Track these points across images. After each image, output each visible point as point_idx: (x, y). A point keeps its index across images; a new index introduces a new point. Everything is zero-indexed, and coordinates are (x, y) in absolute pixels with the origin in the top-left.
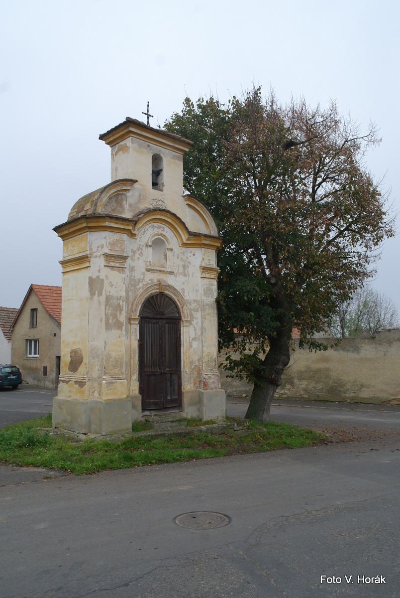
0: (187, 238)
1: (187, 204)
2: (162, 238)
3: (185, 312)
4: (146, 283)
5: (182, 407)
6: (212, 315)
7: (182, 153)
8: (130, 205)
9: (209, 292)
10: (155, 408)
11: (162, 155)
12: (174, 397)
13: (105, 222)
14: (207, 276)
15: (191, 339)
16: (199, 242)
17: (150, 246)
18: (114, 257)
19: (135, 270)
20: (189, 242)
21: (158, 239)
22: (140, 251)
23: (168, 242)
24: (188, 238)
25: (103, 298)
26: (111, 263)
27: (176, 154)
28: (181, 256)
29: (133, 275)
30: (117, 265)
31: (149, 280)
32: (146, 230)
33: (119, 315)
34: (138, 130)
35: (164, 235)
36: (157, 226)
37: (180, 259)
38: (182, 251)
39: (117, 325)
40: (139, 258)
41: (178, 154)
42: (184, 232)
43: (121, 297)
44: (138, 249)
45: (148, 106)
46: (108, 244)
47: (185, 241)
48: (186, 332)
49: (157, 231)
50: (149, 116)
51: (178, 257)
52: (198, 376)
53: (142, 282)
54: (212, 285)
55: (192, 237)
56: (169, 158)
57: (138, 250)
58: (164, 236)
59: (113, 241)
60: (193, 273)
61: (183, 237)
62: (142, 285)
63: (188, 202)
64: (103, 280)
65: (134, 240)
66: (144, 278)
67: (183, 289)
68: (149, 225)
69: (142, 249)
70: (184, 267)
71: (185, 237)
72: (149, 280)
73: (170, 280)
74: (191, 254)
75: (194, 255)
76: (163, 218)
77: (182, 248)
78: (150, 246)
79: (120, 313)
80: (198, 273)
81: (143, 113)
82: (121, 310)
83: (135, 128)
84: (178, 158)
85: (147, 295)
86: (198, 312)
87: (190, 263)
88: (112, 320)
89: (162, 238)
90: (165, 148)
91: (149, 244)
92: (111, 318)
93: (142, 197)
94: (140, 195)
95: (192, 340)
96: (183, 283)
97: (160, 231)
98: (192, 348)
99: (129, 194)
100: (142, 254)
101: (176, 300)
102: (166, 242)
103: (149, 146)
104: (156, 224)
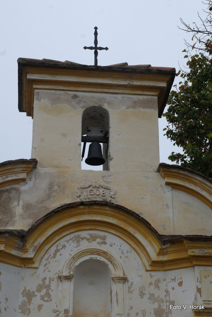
0: (158, 250)
1: (168, 184)
2: (99, 258)
7: (157, 93)
8: (27, 207)
11: (106, 106)
16: (182, 255)
17: (68, 278)
20: (165, 258)
21: (91, 260)
22: (44, 292)
23: (113, 265)
24: (161, 250)
27: (141, 97)
28: (152, 289)
32: (60, 247)
34: (44, 75)
35: (104, 253)
36: (88, 237)
37: (147, 296)
38: (153, 280)
41: (145, 97)
42: (150, 239)
44: (39, 289)
45: (96, 34)
47: (154, 257)
50: (96, 49)
51: (142, 294)
55: (168, 245)
56: (124, 107)
57: (39, 290)
58: (104, 254)
61: (150, 249)
63: (167, 180)
65: (33, 271)
68: (68, 238)
69: (48, 287)
74: (175, 284)
75: (180, 284)
76: (98, 218)
77: (153, 273)
78: (68, 278)
81: (107, 49)
83: (39, 73)
84: (145, 104)
89: (99, 258)
90: (112, 93)
91: (64, 274)
93: (55, 188)
94: (51, 186)
97: (94, 245)
99: (23, 188)
102: (110, 266)
104: (84, 234)
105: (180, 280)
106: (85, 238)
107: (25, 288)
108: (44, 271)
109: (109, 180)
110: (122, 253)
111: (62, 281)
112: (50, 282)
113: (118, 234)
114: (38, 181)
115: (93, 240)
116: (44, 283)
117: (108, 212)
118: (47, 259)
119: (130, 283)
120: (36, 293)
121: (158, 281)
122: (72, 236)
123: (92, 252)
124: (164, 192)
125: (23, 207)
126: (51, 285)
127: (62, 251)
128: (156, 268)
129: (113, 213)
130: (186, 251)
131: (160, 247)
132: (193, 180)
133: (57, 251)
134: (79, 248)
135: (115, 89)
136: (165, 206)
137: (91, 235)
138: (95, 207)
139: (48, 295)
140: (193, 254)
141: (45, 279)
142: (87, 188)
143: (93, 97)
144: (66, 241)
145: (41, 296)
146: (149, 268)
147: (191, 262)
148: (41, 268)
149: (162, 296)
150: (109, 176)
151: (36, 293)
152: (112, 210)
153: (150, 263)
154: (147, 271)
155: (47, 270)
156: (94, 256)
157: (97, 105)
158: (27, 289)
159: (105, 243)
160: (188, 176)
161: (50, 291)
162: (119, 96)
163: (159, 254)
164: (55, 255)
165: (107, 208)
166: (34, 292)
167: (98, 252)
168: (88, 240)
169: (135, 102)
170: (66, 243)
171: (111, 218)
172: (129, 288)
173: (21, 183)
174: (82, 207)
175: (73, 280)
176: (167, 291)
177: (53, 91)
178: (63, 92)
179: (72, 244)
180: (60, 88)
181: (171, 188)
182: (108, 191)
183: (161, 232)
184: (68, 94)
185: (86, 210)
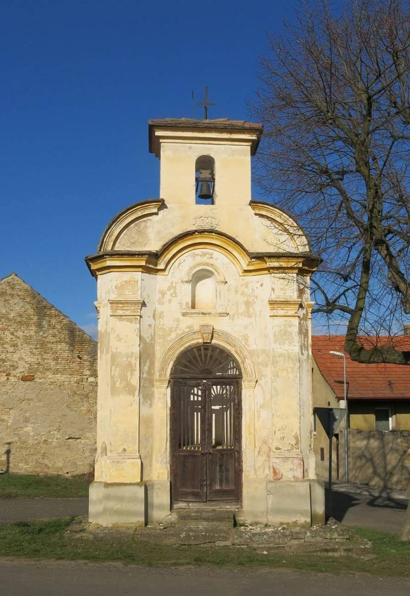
0: (248, 263)
1: (256, 214)
3: (248, 367)
4: (182, 331)
5: (241, 502)
6: (290, 370)
9: (285, 337)
10: (194, 500)
12: (225, 487)
13: (106, 261)
14: (281, 312)
15: (259, 406)
18: (122, 303)
19: (163, 316)
22: (172, 291)
23: (218, 273)
25: (109, 356)
26: (118, 311)
29: (161, 324)
30: (128, 313)
31: (186, 328)
33: (129, 377)
39: (127, 389)
40: (170, 301)
43: (132, 353)
44: (169, 289)
46: (114, 288)
48: (250, 396)
49: (199, 259)
51: (236, 292)
52: (267, 459)
53: (176, 330)
54: (290, 326)
57: (169, 289)
59: (121, 283)
60: (260, 312)
61: (242, 261)
62: (175, 335)
64: (109, 333)
66: (178, 325)
67: (246, 338)
69: (175, 288)
70: (247, 304)
71: (244, 262)
72: (186, 328)
73: (221, 325)
75: (262, 285)
79: (132, 375)
80: (267, 310)
82: (133, 370)
85: (182, 348)
86: (267, 367)
87: (256, 297)
88: (121, 383)
92: (119, 381)
95: (260, 408)
96: (246, 328)
98: (261, 418)
100: (176, 294)
101: (233, 352)
102: (216, 273)
103: (190, 148)
105: (262, 283)
118: (173, 269)
120: (167, 292)
141: (172, 282)
159: (212, 258)
164: (179, 266)
176: (253, 290)
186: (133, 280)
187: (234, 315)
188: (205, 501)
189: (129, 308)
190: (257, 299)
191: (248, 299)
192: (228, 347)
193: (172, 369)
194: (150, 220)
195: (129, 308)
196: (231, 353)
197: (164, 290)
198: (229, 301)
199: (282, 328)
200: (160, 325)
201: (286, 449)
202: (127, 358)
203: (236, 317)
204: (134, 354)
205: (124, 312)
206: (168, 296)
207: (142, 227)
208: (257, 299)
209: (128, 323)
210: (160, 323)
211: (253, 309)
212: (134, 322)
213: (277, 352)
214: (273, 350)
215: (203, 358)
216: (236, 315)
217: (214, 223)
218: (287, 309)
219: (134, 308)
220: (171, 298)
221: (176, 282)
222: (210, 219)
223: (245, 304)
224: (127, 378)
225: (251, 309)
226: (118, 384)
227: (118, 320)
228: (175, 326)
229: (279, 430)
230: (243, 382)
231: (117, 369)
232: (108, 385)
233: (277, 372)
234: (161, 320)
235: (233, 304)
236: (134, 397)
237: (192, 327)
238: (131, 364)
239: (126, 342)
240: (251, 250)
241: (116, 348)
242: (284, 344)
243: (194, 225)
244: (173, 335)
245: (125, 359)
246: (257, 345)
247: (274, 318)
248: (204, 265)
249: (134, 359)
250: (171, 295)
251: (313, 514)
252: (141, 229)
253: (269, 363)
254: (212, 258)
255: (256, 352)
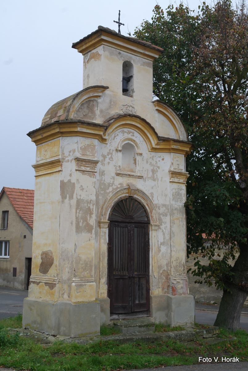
0: (156, 143)
1: (157, 110)
3: (154, 216)
5: (150, 312)
8: (101, 111)
11: (132, 62)
15: (159, 243)
16: (168, 147)
17: (120, 151)
18: (85, 162)
19: (105, 174)
20: (158, 147)
21: (128, 143)
22: (110, 156)
23: (137, 147)
24: (158, 143)
25: (74, 202)
26: (82, 167)
28: (150, 160)
29: (103, 179)
30: (88, 169)
31: (119, 184)
32: (116, 135)
33: (89, 219)
34: (109, 38)
35: (134, 141)
36: (127, 131)
37: (149, 163)
39: (87, 228)
40: (109, 163)
41: (148, 61)
47: (154, 146)
50: (120, 24)
51: (147, 162)
53: (112, 186)
55: (161, 141)
57: (108, 155)
58: (134, 141)
60: (162, 178)
63: (157, 108)
65: (105, 145)
66: (113, 182)
68: (119, 131)
69: (112, 154)
70: (153, 171)
71: (154, 142)
72: (119, 184)
73: (140, 185)
74: (160, 159)
75: (163, 159)
77: (151, 153)
78: (120, 151)
80: (167, 178)
82: (91, 214)
84: (148, 65)
86: (167, 216)
87: (159, 167)
88: (83, 223)
90: (135, 55)
93: (112, 103)
95: (161, 245)
99: (100, 100)
102: (136, 147)
104: (126, 130)
105: (163, 158)
106: (126, 132)
107: (102, 153)
108: (110, 146)
109: (134, 103)
110: (140, 142)
111: (117, 152)
112: (112, 151)
113: (139, 132)
114: (105, 98)
115: (129, 134)
116: (110, 152)
117: (138, 121)
118: (111, 140)
119: (143, 156)
120: (107, 156)
121: (153, 157)
122: (121, 130)
123: (129, 139)
124: (155, 114)
125: (100, 111)
126: (113, 153)
127: (117, 137)
128: (153, 151)
129: (140, 122)
130: (170, 145)
131: (158, 142)
132: (168, 110)
133: (115, 137)
134: (124, 136)
135: (137, 53)
136: (155, 121)
137: (128, 131)
138: (134, 118)
139: (112, 157)
140: (173, 148)
141: (110, 150)
142: (125, 106)
143: (127, 56)
144: (118, 132)
145: (109, 158)
146: (150, 150)
147: (170, 151)
148: (109, 144)
149: (154, 164)
150: (134, 101)
151: (107, 156)
152: (140, 120)
153: (151, 148)
154: (149, 151)
155: (111, 146)
156: (130, 142)
157: (129, 61)
158: (103, 154)
159: (134, 136)
160: (167, 108)
161: (112, 156)
162: (138, 57)
163: (156, 145)
164: (114, 138)
165: (138, 119)
166: (106, 155)
167: (131, 140)
168: (127, 133)
169: (144, 63)
170: (118, 133)
171: (139, 124)
172: (143, 159)
173: (98, 98)
174: (128, 117)
175: (122, 152)
176: (156, 162)
177: (111, 48)
178: (114, 49)
179: (121, 134)
180: (114, 46)
181: (157, 112)
182: (134, 109)
183: (159, 135)
184: (117, 51)
185: (130, 119)
186: (93, 145)
187: (146, 178)
188: (130, 312)
189: (89, 166)
190: (159, 169)
191: (153, 168)
192: (143, 201)
193: (110, 214)
194: (95, 100)
195: (89, 166)
196: (144, 205)
197: (105, 155)
198: (143, 168)
199: (177, 190)
200: (102, 180)
201: (178, 274)
202: (87, 204)
203: (147, 180)
204: (92, 202)
205: (85, 168)
206: (107, 160)
207: (91, 105)
208: (159, 169)
209: (88, 177)
210: (102, 179)
211: (157, 175)
212: (92, 177)
213: (174, 206)
214: (172, 205)
215: (128, 208)
216: (147, 179)
217: (133, 111)
218: (180, 178)
219: (92, 166)
220: (109, 161)
221: (112, 150)
222: (131, 108)
223: (152, 171)
224: (87, 220)
225: (155, 175)
226: (81, 224)
227: (82, 174)
228: (112, 182)
229: (175, 260)
230: (150, 226)
231: (81, 212)
232: (72, 223)
233: (174, 220)
234: (103, 176)
235: (145, 171)
236: (91, 234)
237: (122, 184)
238: (90, 209)
239: (87, 191)
240: (160, 134)
241: (80, 196)
242: (177, 202)
243: (122, 110)
244: (111, 189)
245: (86, 205)
246: (158, 200)
247: (173, 183)
248: (129, 140)
249: (92, 205)
250: (109, 159)
251: (196, 321)
252: (90, 106)
253: (168, 214)
254: (134, 136)
255: (158, 205)
